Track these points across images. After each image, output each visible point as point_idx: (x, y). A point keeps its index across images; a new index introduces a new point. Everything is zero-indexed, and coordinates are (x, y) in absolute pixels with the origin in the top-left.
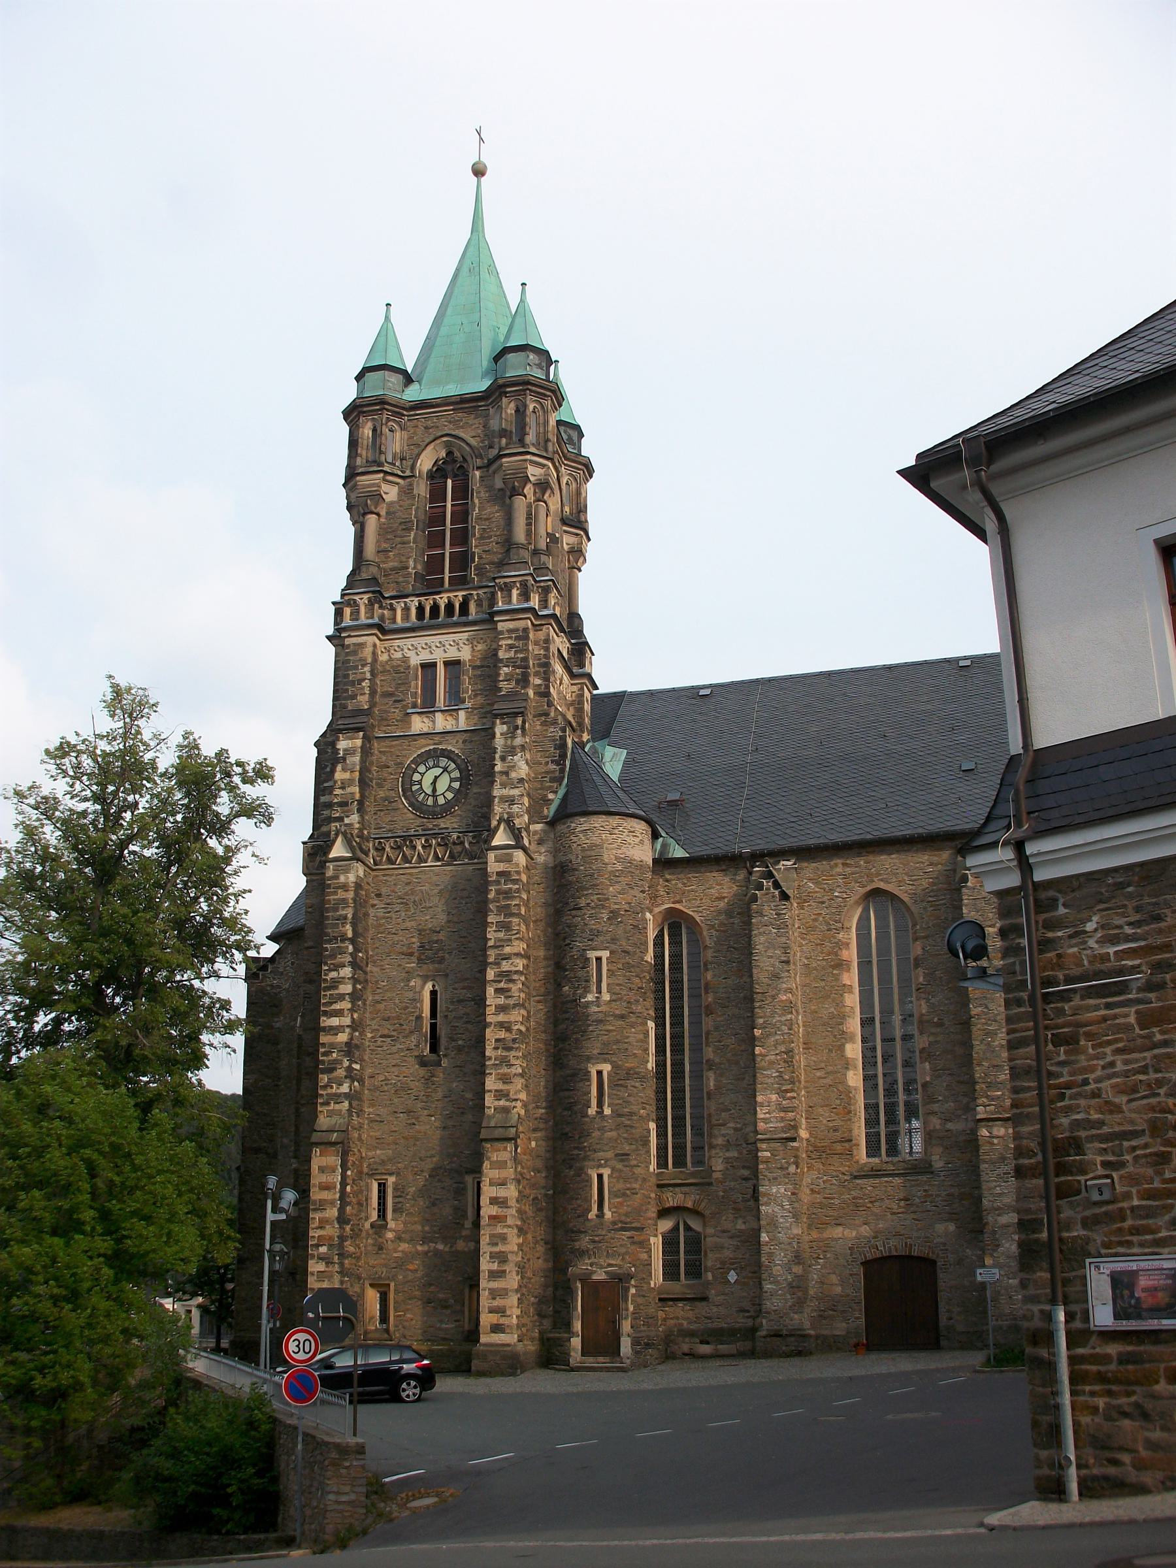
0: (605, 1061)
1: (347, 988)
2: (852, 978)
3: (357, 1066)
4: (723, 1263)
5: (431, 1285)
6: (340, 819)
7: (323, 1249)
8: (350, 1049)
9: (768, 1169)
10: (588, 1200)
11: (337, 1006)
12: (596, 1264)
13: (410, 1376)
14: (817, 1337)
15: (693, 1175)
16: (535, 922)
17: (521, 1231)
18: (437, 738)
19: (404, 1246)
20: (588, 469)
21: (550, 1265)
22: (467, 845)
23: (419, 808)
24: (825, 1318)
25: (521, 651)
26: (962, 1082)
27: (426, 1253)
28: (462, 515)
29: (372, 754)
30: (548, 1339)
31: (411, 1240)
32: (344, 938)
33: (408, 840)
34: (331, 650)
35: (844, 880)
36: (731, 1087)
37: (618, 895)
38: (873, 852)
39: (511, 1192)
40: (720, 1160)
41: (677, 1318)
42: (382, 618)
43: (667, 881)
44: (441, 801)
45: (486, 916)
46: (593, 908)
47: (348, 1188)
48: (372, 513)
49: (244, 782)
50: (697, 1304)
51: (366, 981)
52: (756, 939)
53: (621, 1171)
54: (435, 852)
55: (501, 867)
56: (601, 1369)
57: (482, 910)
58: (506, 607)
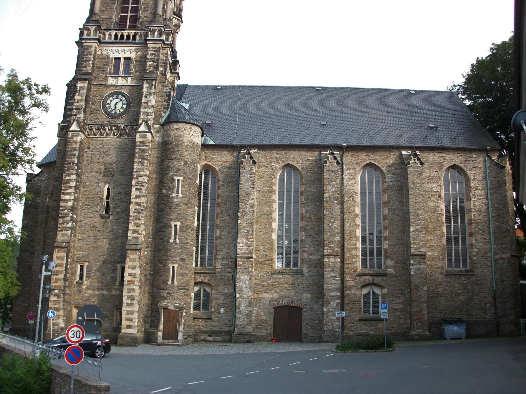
0: (178, 221)
1: (73, 184)
2: (276, 197)
3: (75, 216)
4: (219, 305)
6: (76, 115)
7: (56, 291)
8: (73, 209)
9: (240, 269)
11: (68, 191)
12: (170, 302)
13: (99, 346)
14: (255, 336)
15: (208, 269)
17: (140, 288)
18: (118, 87)
19: (90, 292)
21: (150, 302)
22: (127, 131)
23: (108, 114)
25: (156, 56)
26: (316, 241)
27: (99, 295)
29: (91, 91)
30: (148, 332)
31: (93, 289)
32: (73, 163)
33: (103, 126)
34: (76, 49)
37: (188, 156)
39: (137, 271)
42: (100, 36)
45: (134, 158)
47: (69, 267)
49: (37, 93)
50: (208, 321)
51: (81, 182)
53: (182, 266)
54: (114, 132)
55: (142, 140)
56: (171, 345)
57: (132, 157)
58: (152, 38)
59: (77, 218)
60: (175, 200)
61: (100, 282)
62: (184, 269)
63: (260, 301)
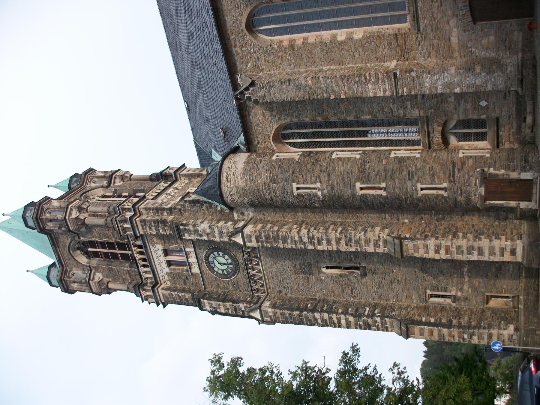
2: (299, 38)
4: (475, 109)
5: (487, 275)
7: (466, 336)
10: (437, 196)
14: (523, 51)
16: (284, 218)
18: (200, 261)
19: (465, 287)
20: (91, 171)
21: (476, 213)
24: (511, 45)
25: (151, 224)
27: (469, 277)
28: (103, 245)
31: (462, 284)
32: (300, 315)
33: (250, 277)
34: (170, 306)
35: (244, 46)
36: (369, 107)
37: (262, 178)
38: (226, 31)
39: (432, 242)
40: (413, 111)
41: (509, 135)
43: (258, 143)
44: (230, 261)
46: (270, 192)
47: (432, 320)
48: (107, 286)
50: (501, 123)
52: (279, 99)
53: (419, 177)
54: (255, 265)
55: (254, 240)
59: (369, 305)
60: (325, 192)
61: (451, 276)
62: (424, 173)
63: (464, 46)
